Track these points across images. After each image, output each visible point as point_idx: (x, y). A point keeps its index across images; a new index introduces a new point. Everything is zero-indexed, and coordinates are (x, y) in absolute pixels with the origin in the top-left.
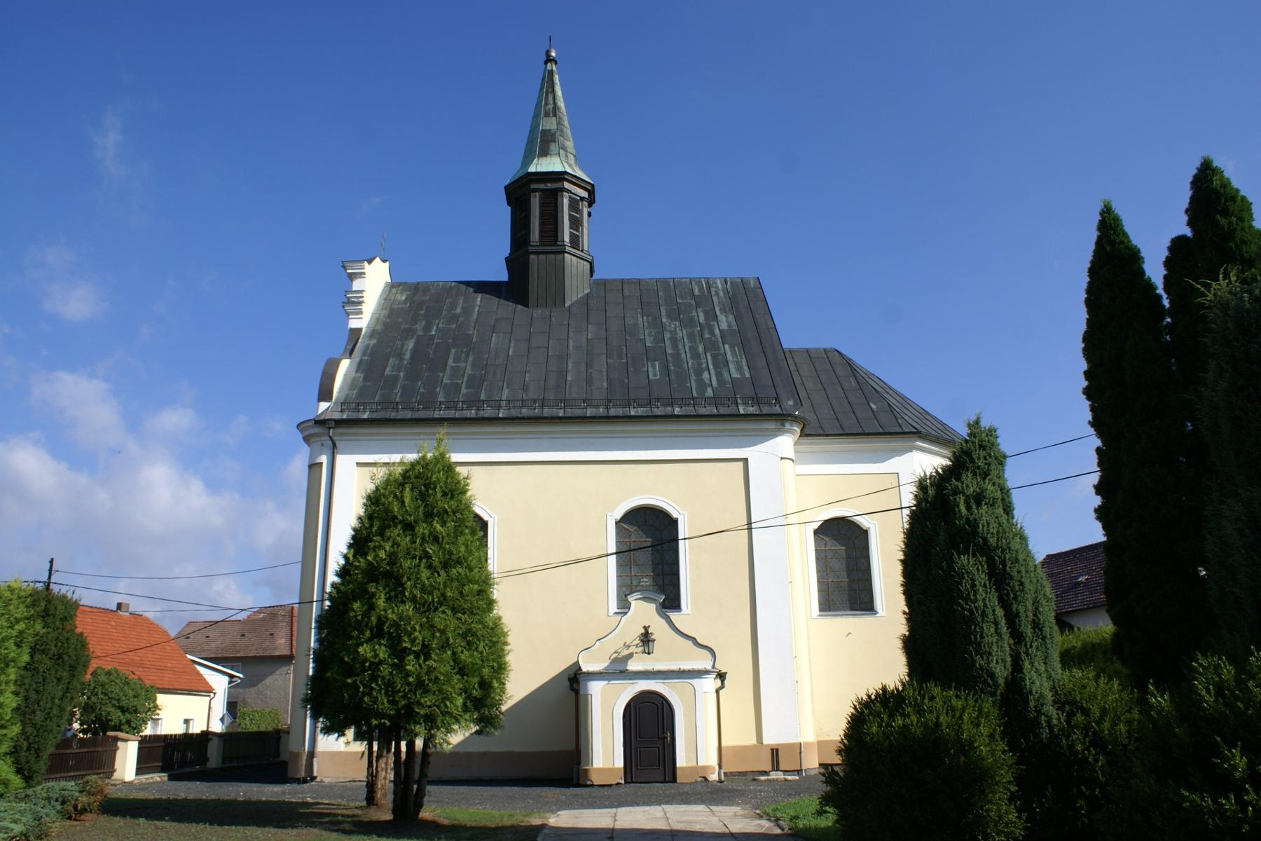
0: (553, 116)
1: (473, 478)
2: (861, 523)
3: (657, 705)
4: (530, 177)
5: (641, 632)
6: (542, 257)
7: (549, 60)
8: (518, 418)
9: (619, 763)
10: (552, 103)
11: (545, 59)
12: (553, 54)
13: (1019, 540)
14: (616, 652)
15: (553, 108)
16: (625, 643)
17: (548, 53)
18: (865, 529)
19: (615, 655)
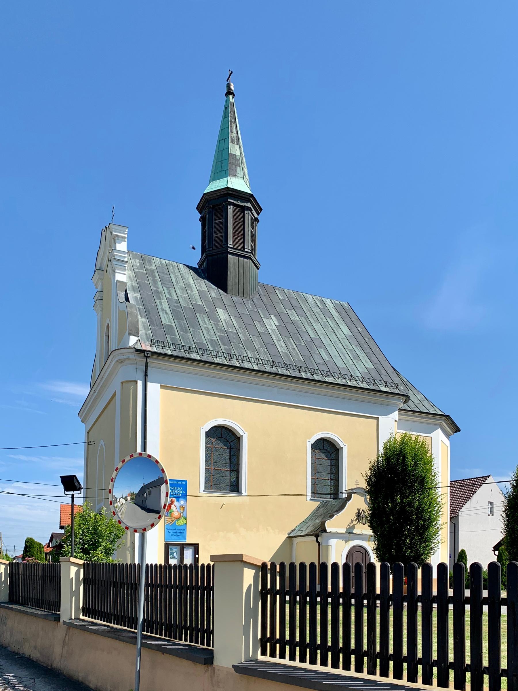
0: (237, 144)
1: (435, 459)
2: (220, 424)
3: (363, 554)
4: (229, 192)
5: (38, 539)
6: (236, 258)
7: (229, 93)
8: (182, 358)
9: (289, 600)
10: (235, 132)
11: (226, 91)
12: (232, 87)
13: (420, 466)
14: (348, 525)
15: (236, 137)
16: (352, 519)
17: (228, 85)
18: (238, 436)
19: (348, 527)
